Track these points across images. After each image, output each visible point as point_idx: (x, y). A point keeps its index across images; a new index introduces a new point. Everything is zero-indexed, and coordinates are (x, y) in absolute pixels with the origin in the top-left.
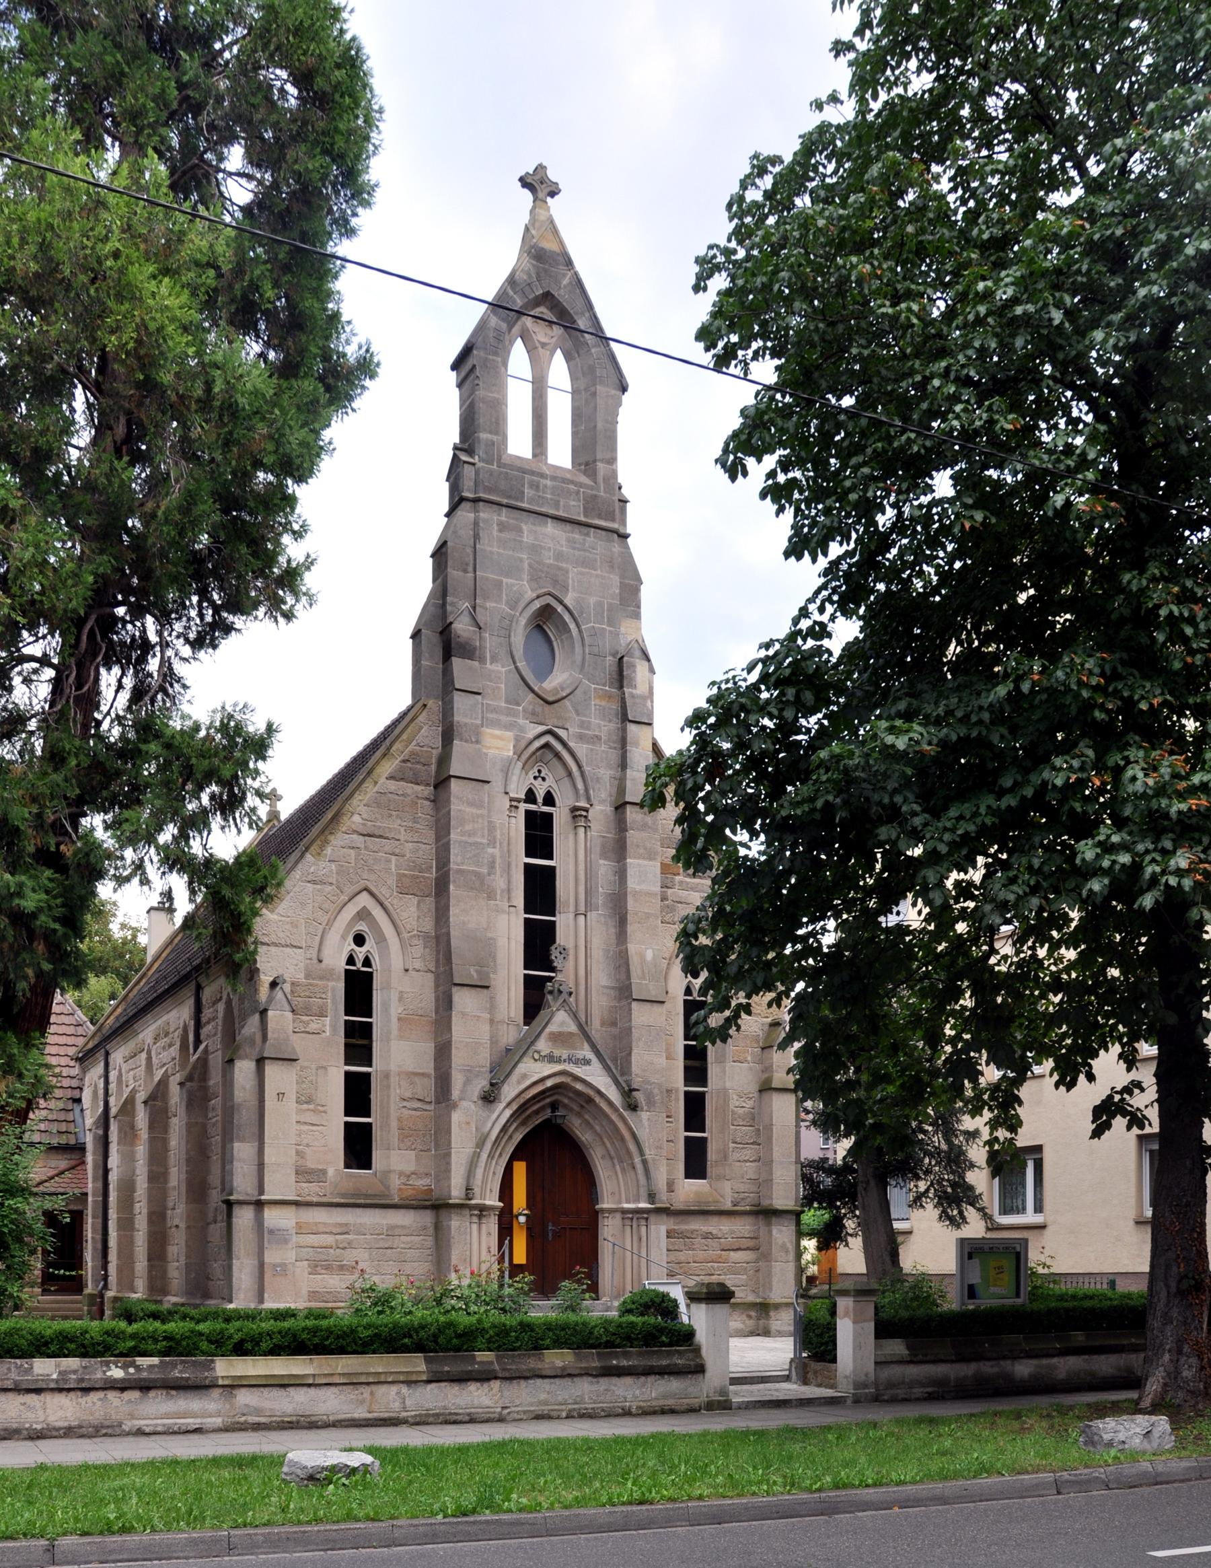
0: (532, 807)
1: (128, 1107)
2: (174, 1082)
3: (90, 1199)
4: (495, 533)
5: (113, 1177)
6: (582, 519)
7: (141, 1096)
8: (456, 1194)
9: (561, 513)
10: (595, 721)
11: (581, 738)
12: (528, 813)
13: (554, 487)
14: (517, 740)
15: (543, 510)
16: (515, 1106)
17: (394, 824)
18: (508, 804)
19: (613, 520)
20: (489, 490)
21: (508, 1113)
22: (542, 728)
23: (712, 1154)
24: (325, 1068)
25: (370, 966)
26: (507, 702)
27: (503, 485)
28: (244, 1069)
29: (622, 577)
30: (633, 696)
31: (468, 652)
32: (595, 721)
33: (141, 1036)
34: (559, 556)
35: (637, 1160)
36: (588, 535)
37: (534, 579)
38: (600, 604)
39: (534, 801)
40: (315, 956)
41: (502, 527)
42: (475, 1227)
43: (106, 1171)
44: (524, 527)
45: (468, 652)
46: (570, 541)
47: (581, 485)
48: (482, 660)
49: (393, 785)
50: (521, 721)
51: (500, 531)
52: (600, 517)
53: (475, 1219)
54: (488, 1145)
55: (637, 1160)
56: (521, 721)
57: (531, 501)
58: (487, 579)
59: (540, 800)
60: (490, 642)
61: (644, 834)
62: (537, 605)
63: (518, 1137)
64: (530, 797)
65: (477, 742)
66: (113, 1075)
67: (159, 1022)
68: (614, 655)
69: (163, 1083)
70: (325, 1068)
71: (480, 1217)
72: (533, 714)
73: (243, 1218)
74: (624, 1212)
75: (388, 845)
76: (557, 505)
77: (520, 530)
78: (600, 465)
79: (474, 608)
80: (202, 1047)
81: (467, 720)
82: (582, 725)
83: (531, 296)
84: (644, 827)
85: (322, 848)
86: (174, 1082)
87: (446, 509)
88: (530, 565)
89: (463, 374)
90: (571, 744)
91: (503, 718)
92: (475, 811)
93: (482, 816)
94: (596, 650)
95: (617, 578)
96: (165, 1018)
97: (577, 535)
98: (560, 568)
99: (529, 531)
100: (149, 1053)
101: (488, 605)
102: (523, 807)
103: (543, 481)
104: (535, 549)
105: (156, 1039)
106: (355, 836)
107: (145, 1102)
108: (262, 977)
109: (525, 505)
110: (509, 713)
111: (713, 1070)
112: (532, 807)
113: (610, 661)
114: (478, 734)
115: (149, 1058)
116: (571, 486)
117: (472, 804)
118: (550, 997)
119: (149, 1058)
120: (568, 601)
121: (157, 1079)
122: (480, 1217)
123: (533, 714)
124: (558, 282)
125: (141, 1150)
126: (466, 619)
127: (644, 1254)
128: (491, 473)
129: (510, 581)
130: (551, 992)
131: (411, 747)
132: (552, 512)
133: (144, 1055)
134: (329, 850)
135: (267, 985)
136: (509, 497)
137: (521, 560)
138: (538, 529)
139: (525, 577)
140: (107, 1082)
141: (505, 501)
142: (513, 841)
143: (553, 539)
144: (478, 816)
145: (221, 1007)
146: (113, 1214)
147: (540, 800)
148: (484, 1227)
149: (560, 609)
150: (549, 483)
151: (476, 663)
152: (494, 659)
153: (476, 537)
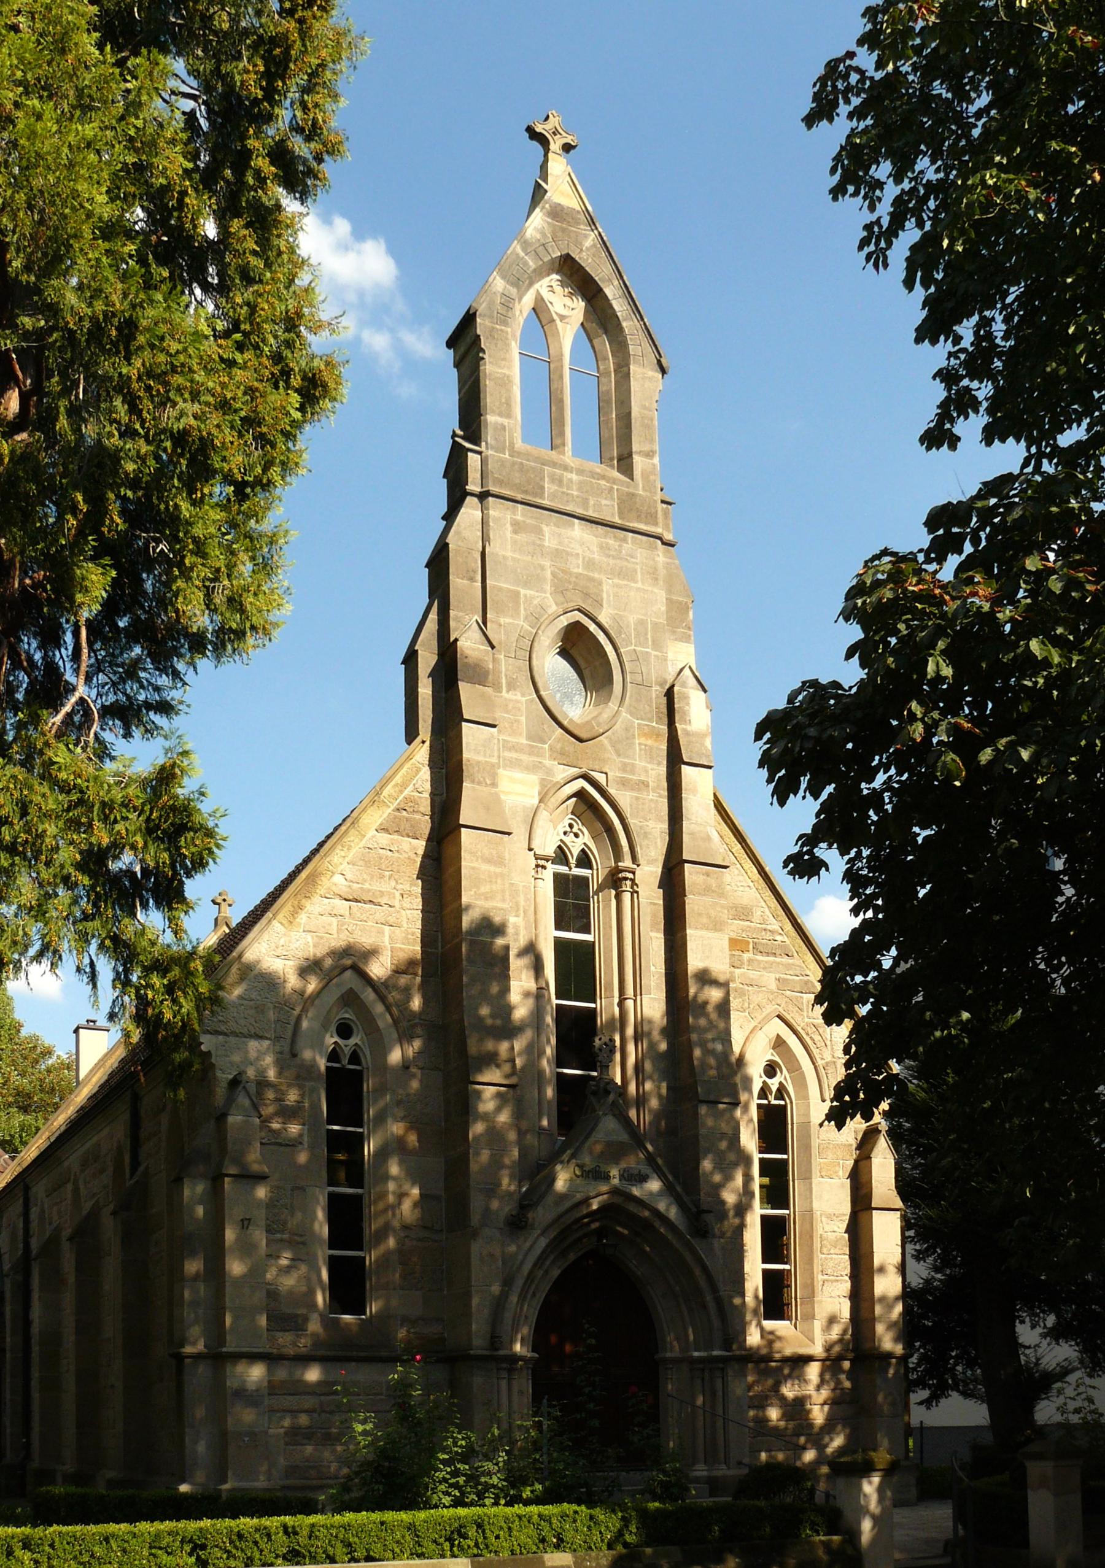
0: (563, 869)
1: (51, 1246)
2: (106, 1212)
3: (8, 1355)
4: (509, 534)
5: (35, 1329)
6: (617, 520)
7: (66, 1233)
8: (478, 1343)
9: (591, 513)
10: (640, 763)
11: (624, 783)
12: (558, 878)
13: (580, 482)
14: (543, 782)
15: (569, 508)
16: (553, 1234)
17: (386, 886)
18: (533, 862)
19: (656, 524)
20: (501, 483)
21: (543, 1242)
22: (574, 771)
23: (797, 1289)
24: (303, 1189)
25: (359, 1063)
26: (529, 738)
27: (517, 477)
28: (194, 1190)
29: (669, 591)
30: (687, 733)
31: (480, 676)
32: (640, 763)
33: (66, 1164)
34: (590, 564)
35: (709, 1298)
36: (625, 540)
37: (560, 590)
38: (641, 623)
39: (566, 863)
40: (287, 1049)
41: (517, 527)
42: (504, 1384)
43: (27, 1323)
44: (545, 529)
45: (480, 676)
46: (603, 548)
47: (614, 481)
48: (497, 687)
49: (384, 839)
50: (547, 762)
51: (515, 532)
52: (639, 519)
53: (505, 1374)
54: (519, 1283)
55: (709, 1298)
56: (547, 762)
57: (553, 496)
58: (500, 589)
59: (573, 861)
60: (506, 666)
61: (708, 900)
62: (564, 621)
63: (556, 1273)
64: (561, 855)
65: (494, 785)
66: (34, 1212)
67: (88, 1145)
68: (661, 685)
69: (93, 1217)
70: (303, 1189)
71: (510, 1371)
72: (562, 753)
73: (199, 1376)
74: (693, 1361)
75: (379, 913)
76: (585, 503)
77: (539, 532)
78: (636, 458)
79: (485, 622)
80: (141, 1169)
81: (481, 758)
82: (624, 768)
83: (547, 259)
84: (707, 890)
85: (294, 914)
86: (106, 1212)
87: (444, 509)
88: (553, 574)
89: (462, 349)
90: (612, 791)
91: (525, 758)
92: (492, 868)
93: (502, 875)
94: (639, 679)
95: (663, 593)
96: (95, 1139)
97: (611, 539)
98: (592, 580)
99: (552, 533)
100: (76, 1182)
101: (502, 620)
102: (552, 868)
103: (568, 475)
104: (558, 554)
105: (84, 1164)
106: (337, 902)
107: (70, 1239)
108: (219, 1074)
109: (545, 502)
110: (532, 751)
111: (796, 1189)
112: (563, 869)
113: (657, 693)
114: (494, 776)
115: (76, 1190)
116: (603, 482)
117: (488, 861)
118: (593, 1099)
119: (76, 1190)
120: (603, 619)
121: (84, 1212)
122: (510, 1371)
123: (562, 753)
124: (579, 244)
125: (68, 1299)
126: (476, 634)
127: (721, 1412)
128: (502, 462)
129: (529, 592)
130: (594, 1093)
131: (406, 793)
132: (580, 511)
133: (70, 1186)
134: (302, 918)
135: (224, 1084)
136: (526, 492)
137: (543, 568)
138: (562, 531)
139: (548, 588)
140: (27, 1221)
141: (519, 497)
142: (540, 908)
143: (582, 544)
144: (497, 875)
145: (165, 1119)
146: (35, 1374)
147: (573, 861)
148: (515, 1383)
149: (592, 627)
150: (574, 477)
151: (489, 690)
152: (511, 686)
153: (485, 538)
